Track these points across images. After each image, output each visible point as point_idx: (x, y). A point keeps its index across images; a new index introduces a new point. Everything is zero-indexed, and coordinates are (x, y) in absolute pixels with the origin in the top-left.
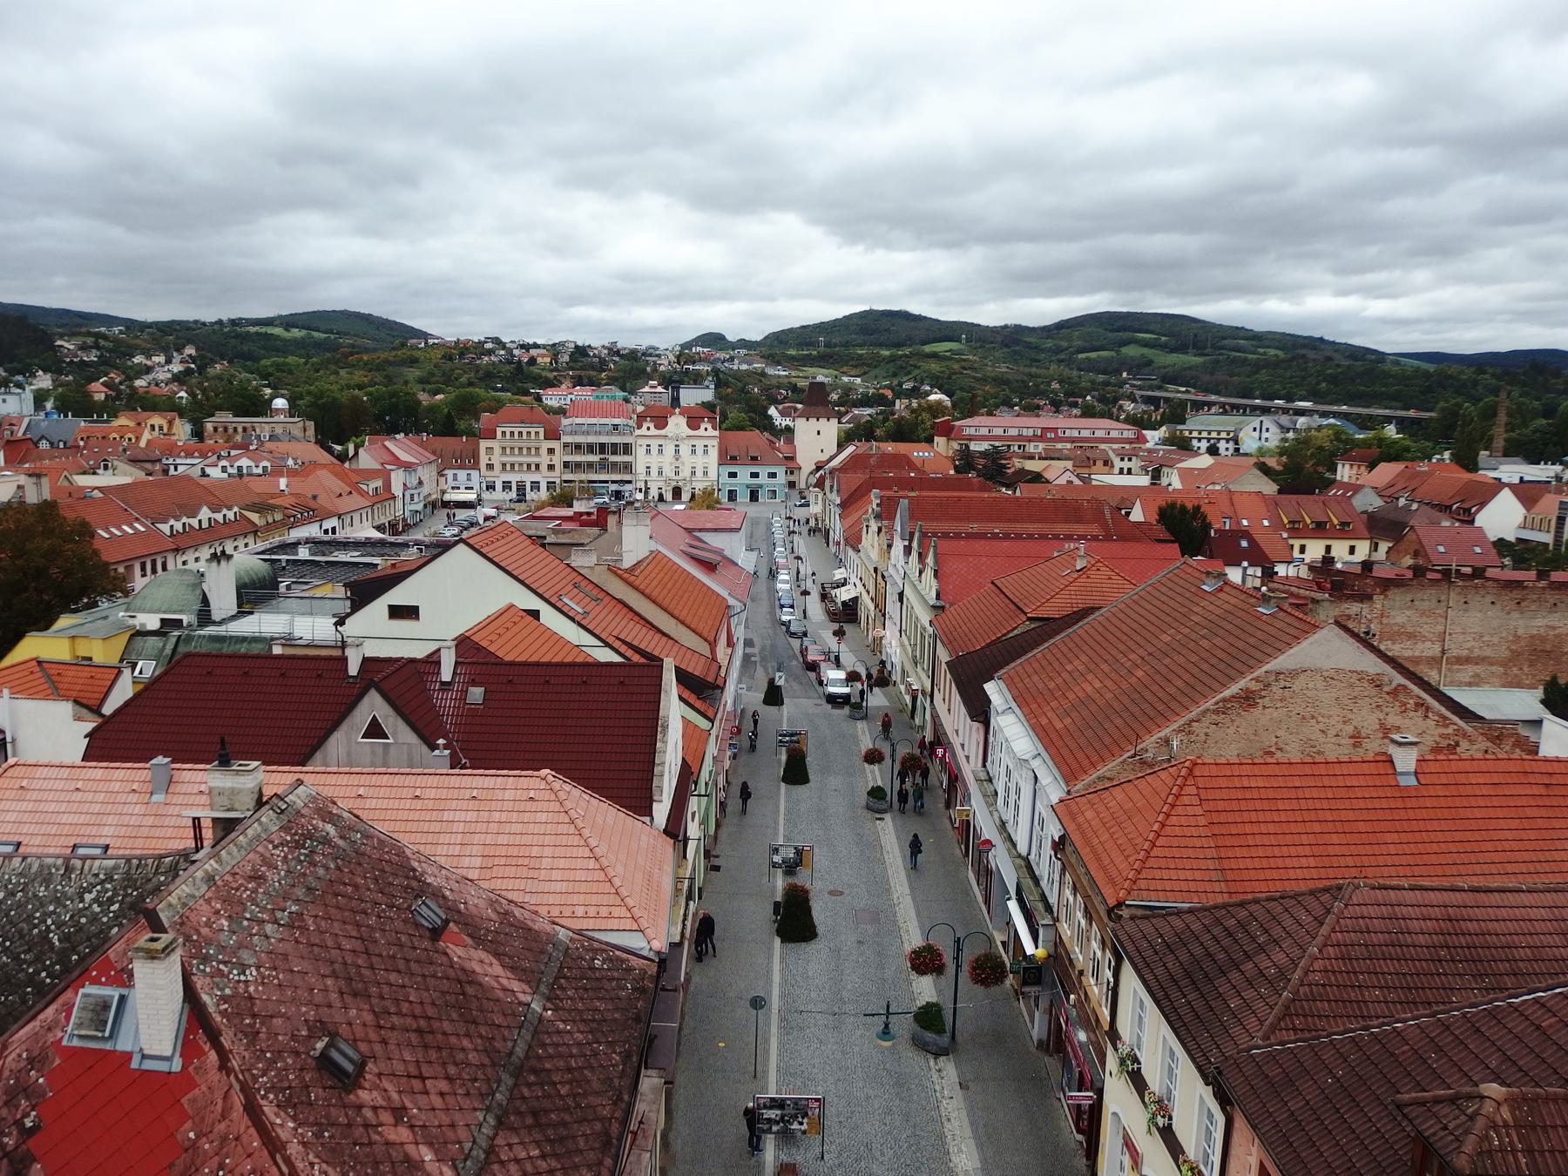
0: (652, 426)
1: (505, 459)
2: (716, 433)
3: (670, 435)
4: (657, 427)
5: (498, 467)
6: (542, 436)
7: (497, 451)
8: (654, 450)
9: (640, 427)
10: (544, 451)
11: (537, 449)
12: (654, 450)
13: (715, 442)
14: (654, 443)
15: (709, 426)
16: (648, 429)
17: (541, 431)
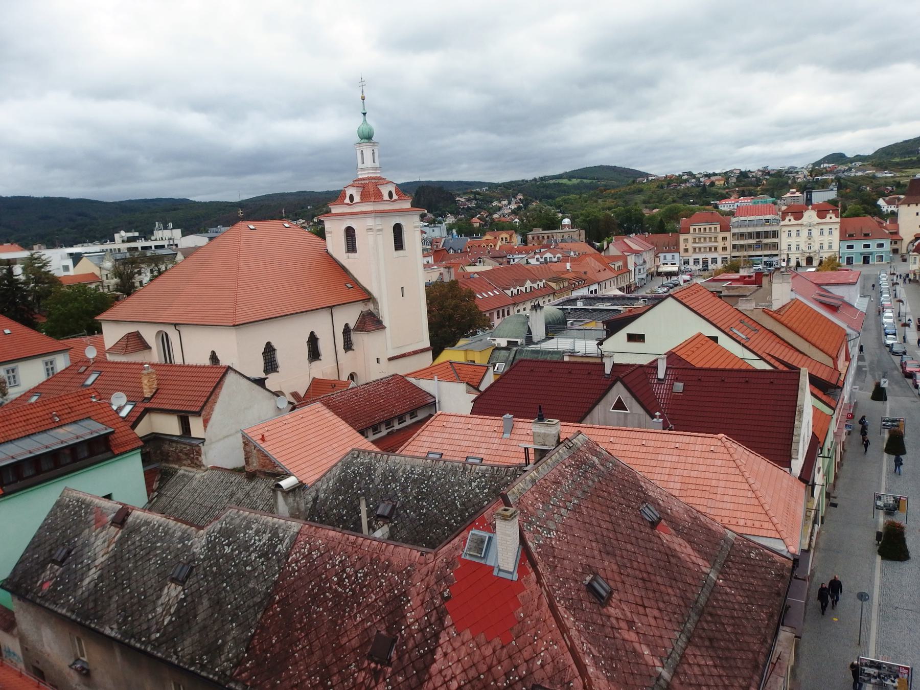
0: (792, 218)
1: (695, 245)
2: (838, 220)
3: (805, 223)
4: (795, 219)
5: (691, 250)
6: (718, 230)
7: (691, 240)
8: (794, 234)
9: (783, 219)
10: (720, 239)
11: (716, 238)
12: (794, 234)
13: (838, 226)
14: (794, 230)
15: (833, 216)
16: (790, 220)
17: (718, 227)
